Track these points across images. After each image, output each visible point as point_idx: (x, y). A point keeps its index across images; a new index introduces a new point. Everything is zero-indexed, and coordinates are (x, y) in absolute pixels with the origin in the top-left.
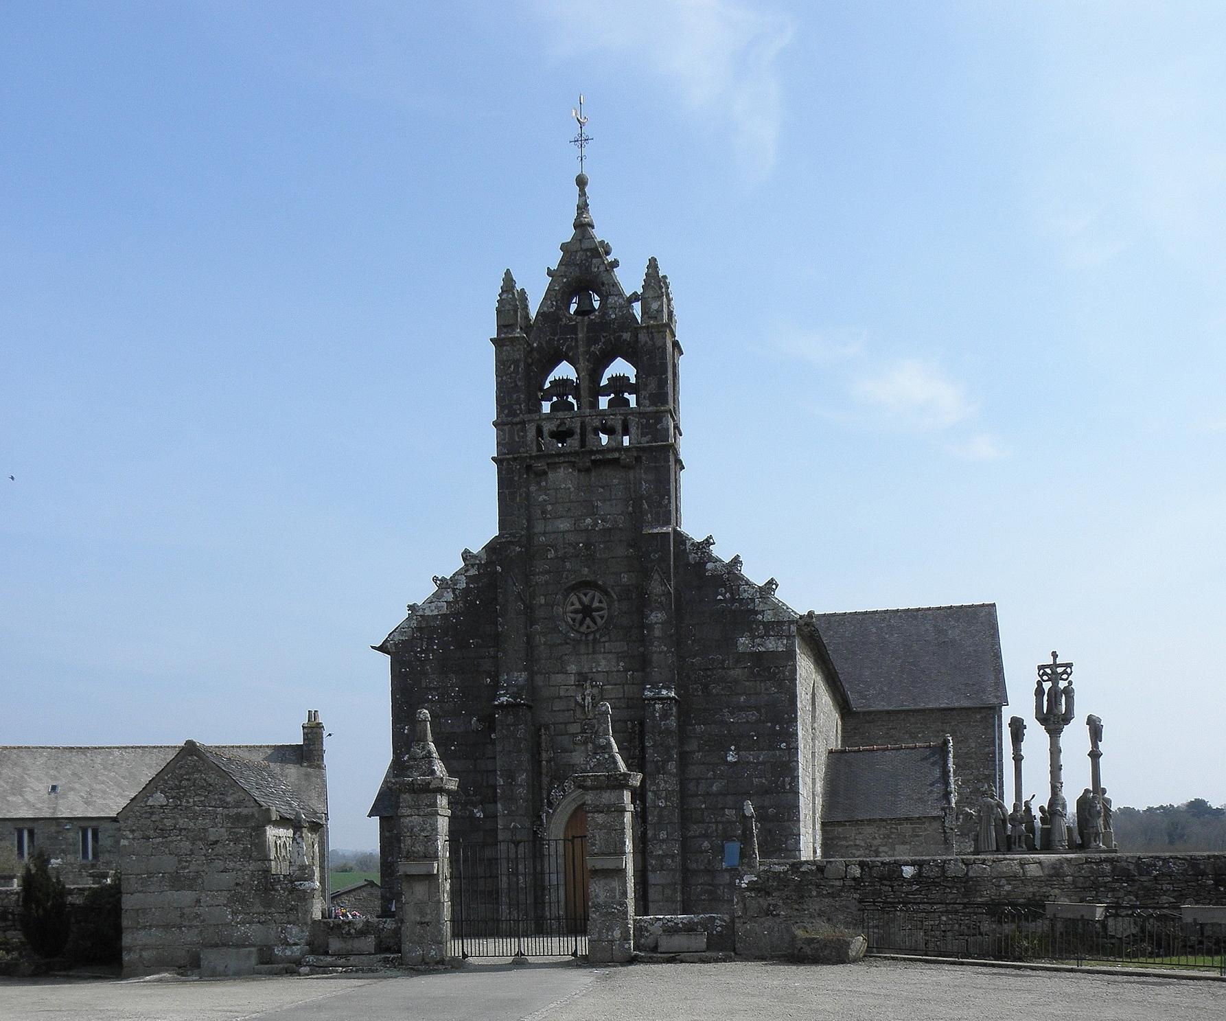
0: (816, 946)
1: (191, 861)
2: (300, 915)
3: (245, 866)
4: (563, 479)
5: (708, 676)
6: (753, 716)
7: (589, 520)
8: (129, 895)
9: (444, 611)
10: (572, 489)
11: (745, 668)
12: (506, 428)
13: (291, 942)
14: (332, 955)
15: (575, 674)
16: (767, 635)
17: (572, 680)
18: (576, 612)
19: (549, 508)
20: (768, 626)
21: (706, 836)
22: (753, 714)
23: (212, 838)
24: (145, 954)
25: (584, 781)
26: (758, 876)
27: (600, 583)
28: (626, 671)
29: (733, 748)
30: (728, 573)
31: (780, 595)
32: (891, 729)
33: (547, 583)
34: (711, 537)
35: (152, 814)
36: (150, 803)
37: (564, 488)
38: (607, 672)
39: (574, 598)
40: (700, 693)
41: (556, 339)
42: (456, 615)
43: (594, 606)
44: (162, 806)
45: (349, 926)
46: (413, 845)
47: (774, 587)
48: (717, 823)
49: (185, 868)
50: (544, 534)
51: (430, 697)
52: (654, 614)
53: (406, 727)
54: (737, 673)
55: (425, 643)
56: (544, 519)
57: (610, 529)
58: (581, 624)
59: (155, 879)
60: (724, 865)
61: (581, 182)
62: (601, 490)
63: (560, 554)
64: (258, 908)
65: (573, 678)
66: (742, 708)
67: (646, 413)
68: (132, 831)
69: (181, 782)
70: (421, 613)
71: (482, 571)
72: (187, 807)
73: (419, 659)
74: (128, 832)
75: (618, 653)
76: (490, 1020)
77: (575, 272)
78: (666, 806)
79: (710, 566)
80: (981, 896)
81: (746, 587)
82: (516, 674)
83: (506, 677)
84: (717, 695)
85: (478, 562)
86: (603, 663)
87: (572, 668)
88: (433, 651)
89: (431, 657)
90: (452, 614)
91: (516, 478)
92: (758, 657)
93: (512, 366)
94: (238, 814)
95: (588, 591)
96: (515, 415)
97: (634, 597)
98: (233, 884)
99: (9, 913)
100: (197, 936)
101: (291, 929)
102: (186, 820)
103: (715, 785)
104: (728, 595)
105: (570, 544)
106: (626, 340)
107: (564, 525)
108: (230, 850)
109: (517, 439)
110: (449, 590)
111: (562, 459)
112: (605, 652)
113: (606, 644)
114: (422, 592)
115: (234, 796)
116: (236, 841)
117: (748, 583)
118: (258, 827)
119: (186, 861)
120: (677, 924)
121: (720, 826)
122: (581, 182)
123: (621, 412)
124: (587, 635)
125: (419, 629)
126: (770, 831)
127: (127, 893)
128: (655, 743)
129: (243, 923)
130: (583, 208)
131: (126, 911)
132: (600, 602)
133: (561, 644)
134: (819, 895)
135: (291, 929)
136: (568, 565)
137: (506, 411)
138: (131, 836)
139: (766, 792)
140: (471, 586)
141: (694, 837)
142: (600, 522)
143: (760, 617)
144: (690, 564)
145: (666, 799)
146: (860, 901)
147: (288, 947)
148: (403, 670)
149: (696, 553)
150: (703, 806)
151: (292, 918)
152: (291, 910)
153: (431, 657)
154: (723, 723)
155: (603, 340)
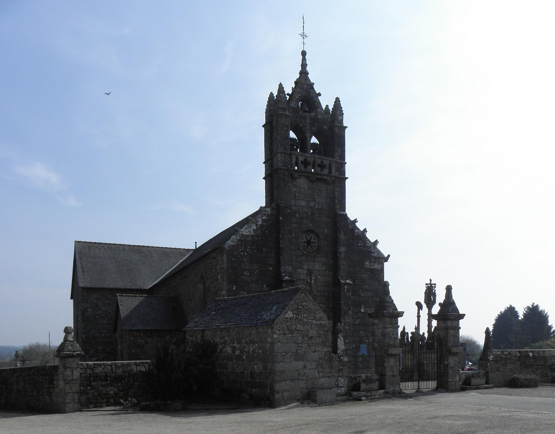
0: (528, 381)
1: (302, 347)
2: (344, 373)
3: (322, 350)
7: (312, 203)
8: (278, 363)
9: (252, 233)
10: (306, 189)
11: (367, 274)
13: (340, 386)
14: (363, 391)
15: (306, 270)
16: (374, 262)
17: (305, 272)
19: (297, 194)
22: (370, 293)
23: (310, 335)
24: (284, 394)
25: (450, 316)
26: (494, 356)
28: (326, 271)
29: (363, 306)
31: (379, 246)
34: (356, 219)
35: (287, 321)
36: (286, 316)
37: (303, 187)
38: (318, 270)
41: (298, 120)
44: (291, 318)
45: (360, 378)
47: (377, 243)
49: (300, 350)
50: (295, 206)
51: (245, 273)
52: (341, 248)
53: (234, 287)
55: (243, 248)
58: (307, 248)
59: (288, 355)
60: (360, 354)
62: (317, 191)
64: (328, 370)
65: (305, 271)
67: (338, 162)
68: (279, 330)
69: (298, 306)
71: (268, 218)
72: (301, 319)
73: (240, 255)
74: (277, 331)
76: (65, 433)
80: (548, 363)
81: (368, 242)
82: (287, 267)
83: (283, 268)
85: (267, 213)
86: (317, 266)
87: (305, 267)
88: (247, 252)
89: (246, 255)
91: (287, 179)
93: (286, 127)
94: (321, 324)
95: (310, 234)
97: (329, 239)
98: (318, 358)
99: (109, 376)
100: (304, 384)
101: (341, 379)
102: (300, 326)
103: (357, 321)
104: (362, 244)
106: (324, 129)
107: (303, 203)
108: (317, 341)
109: (287, 161)
110: (254, 224)
111: (305, 174)
112: (318, 262)
115: (319, 315)
116: (320, 337)
117: (369, 240)
118: (328, 330)
119: (300, 347)
120: (469, 374)
121: (359, 338)
122: (304, 54)
123: (330, 160)
124: (310, 253)
125: (241, 240)
127: (277, 363)
129: (322, 377)
130: (304, 65)
131: (276, 372)
132: (314, 239)
134: (510, 363)
135: (341, 379)
136: (304, 221)
138: (278, 333)
140: (264, 224)
143: (373, 254)
145: (348, 326)
146: (521, 365)
147: (339, 388)
148: (233, 259)
149: (352, 225)
151: (341, 374)
152: (340, 370)
153: (246, 255)
155: (316, 126)
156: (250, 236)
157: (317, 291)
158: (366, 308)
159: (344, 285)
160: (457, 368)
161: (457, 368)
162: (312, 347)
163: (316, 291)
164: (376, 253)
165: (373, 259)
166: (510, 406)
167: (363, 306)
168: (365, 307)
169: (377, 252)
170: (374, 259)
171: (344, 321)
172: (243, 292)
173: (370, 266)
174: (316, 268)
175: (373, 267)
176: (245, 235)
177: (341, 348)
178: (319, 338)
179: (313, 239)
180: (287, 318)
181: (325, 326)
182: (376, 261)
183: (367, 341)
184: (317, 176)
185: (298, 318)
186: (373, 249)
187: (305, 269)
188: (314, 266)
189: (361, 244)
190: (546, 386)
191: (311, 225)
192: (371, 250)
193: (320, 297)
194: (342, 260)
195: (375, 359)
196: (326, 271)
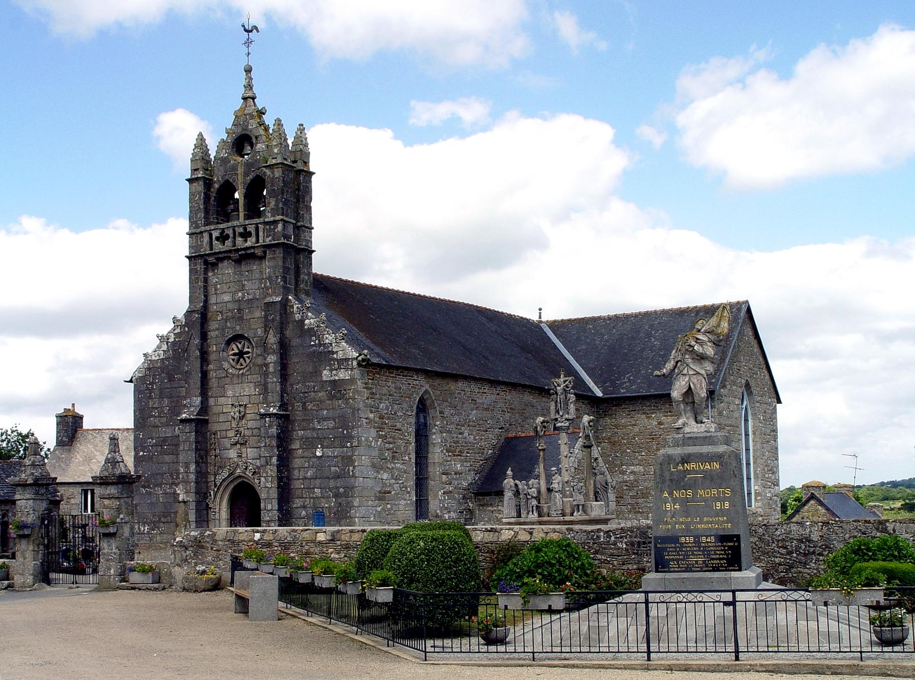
5: (306, 397)
6: (331, 424)
18: (235, 354)
21: (304, 507)
22: (331, 423)
27: (246, 335)
29: (319, 446)
32: (632, 411)
33: (217, 336)
39: (234, 346)
43: (245, 350)
46: (21, 517)
48: (310, 498)
56: (216, 294)
57: (251, 299)
61: (248, 70)
62: (247, 273)
70: (150, 358)
77: (239, 131)
78: (272, 487)
79: (307, 322)
84: (311, 409)
87: (230, 393)
90: (166, 359)
92: (334, 383)
96: (198, 227)
104: (317, 341)
105: (229, 310)
107: (227, 298)
113: (249, 376)
122: (248, 70)
125: (149, 369)
126: (340, 504)
128: (266, 444)
130: (249, 87)
133: (224, 377)
137: (194, 225)
139: (339, 477)
141: (296, 508)
144: (295, 321)
149: (299, 314)
150: (302, 486)
154: (314, 429)
165: (336, 363)
166: (173, 604)
167: (319, 446)
168: (323, 447)
173: (331, 376)
175: (337, 378)
179: (233, 352)
182: (342, 367)
183: (326, 505)
184: (240, 253)
191: (238, 328)
194: (270, 376)
196: (260, 395)
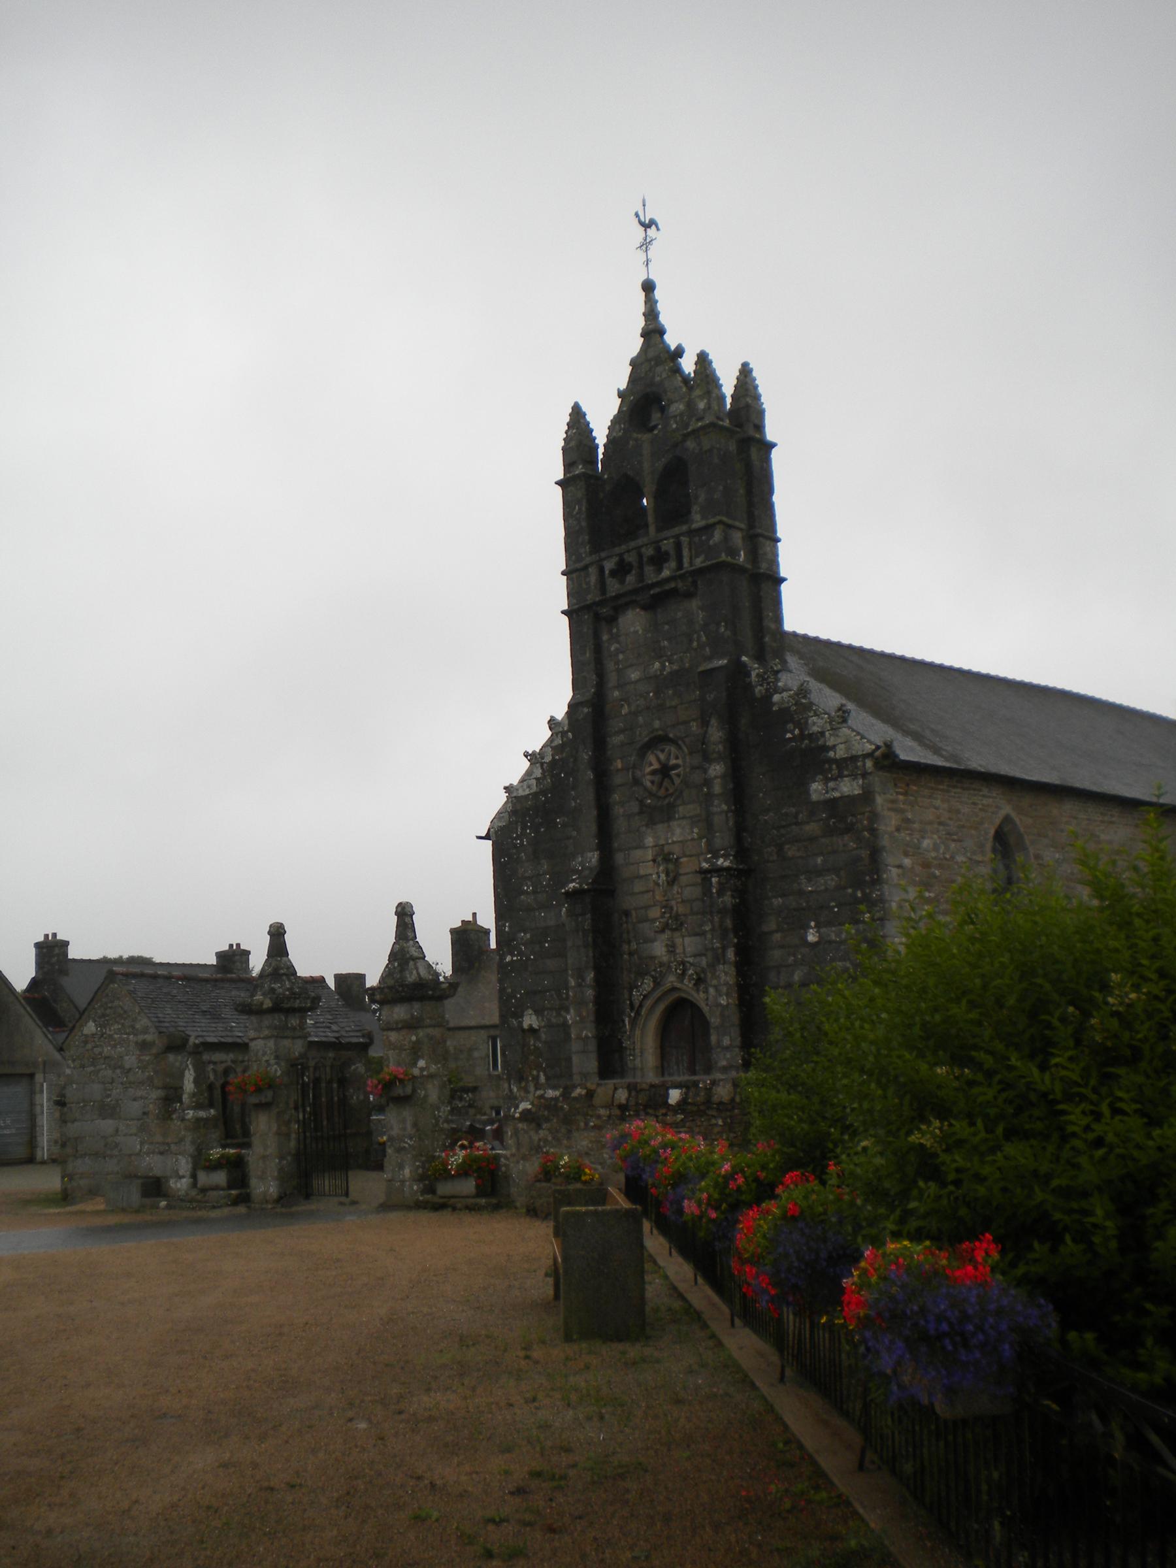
4: (633, 622)
6: (831, 881)
10: (640, 632)
12: (574, 575)
16: (841, 776)
18: (654, 773)
20: (842, 763)
22: (832, 879)
26: (532, 1104)
28: (700, 838)
29: (813, 924)
30: (796, 704)
39: (651, 758)
40: (775, 858)
42: (542, 792)
52: (713, 767)
53: (507, 924)
54: (812, 828)
63: (633, 708)
66: (820, 872)
68: (74, 1061)
73: (515, 846)
75: (691, 817)
86: (678, 831)
87: (649, 841)
92: (832, 805)
95: (665, 747)
114: (516, 770)
122: (648, 287)
129: (148, 1154)
130: (651, 314)
138: (72, 1066)
140: (557, 757)
142: (667, 664)
143: (831, 754)
149: (761, 685)
154: (801, 893)
156: (531, 797)
157: (683, 901)
158: (823, 930)
159: (709, 876)
160: (406, 1143)
161: (409, 1141)
162: (130, 1089)
163: (680, 900)
164: (842, 746)
165: (834, 766)
168: (818, 926)
169: (845, 743)
170: (838, 767)
171: (715, 982)
172: (522, 934)
174: (675, 839)
176: (522, 796)
177: (188, 1090)
178: (142, 1072)
180: (86, 1036)
181: (152, 1044)
182: (846, 773)
185: (105, 1033)
186: (832, 738)
187: (649, 847)
188: (669, 834)
189: (792, 732)
190: (446, 1215)
192: (825, 742)
193: (690, 917)
195: (510, 1111)
